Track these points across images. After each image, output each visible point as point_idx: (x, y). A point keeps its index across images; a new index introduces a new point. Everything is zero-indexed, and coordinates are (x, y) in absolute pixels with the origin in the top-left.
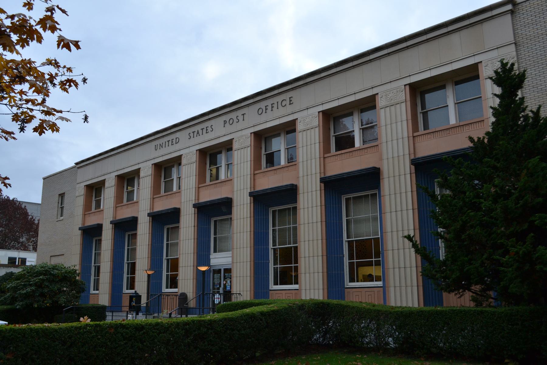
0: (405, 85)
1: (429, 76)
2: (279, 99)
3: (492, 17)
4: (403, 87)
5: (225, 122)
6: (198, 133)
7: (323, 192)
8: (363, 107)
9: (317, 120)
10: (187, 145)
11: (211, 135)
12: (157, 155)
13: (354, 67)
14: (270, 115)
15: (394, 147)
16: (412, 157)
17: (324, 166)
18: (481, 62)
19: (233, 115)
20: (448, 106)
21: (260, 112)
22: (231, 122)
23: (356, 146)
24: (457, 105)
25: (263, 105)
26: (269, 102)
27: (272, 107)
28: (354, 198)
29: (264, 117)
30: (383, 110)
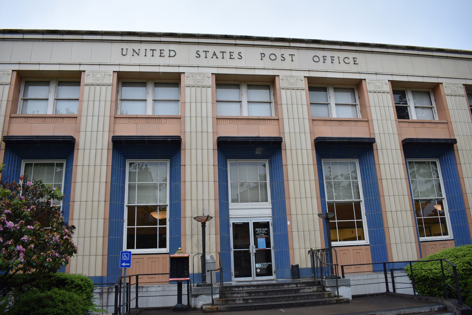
0: (13, 71)
1: (138, 71)
2: (342, 55)
3: (23, 40)
4: (11, 71)
5: (263, 55)
6: (215, 54)
7: (111, 152)
8: (125, 81)
9: (10, 78)
10: (157, 63)
11: (236, 63)
12: (132, 62)
13: (418, 55)
14: (328, 65)
15: (397, 120)
16: (5, 134)
17: (112, 128)
18: (85, 71)
19: (278, 52)
20: (48, 99)
21: (315, 60)
22: (273, 58)
23: (18, 113)
24: (56, 101)
25: (320, 54)
26: (328, 54)
27: (324, 59)
28: (36, 165)
29: (320, 66)
30: (87, 88)
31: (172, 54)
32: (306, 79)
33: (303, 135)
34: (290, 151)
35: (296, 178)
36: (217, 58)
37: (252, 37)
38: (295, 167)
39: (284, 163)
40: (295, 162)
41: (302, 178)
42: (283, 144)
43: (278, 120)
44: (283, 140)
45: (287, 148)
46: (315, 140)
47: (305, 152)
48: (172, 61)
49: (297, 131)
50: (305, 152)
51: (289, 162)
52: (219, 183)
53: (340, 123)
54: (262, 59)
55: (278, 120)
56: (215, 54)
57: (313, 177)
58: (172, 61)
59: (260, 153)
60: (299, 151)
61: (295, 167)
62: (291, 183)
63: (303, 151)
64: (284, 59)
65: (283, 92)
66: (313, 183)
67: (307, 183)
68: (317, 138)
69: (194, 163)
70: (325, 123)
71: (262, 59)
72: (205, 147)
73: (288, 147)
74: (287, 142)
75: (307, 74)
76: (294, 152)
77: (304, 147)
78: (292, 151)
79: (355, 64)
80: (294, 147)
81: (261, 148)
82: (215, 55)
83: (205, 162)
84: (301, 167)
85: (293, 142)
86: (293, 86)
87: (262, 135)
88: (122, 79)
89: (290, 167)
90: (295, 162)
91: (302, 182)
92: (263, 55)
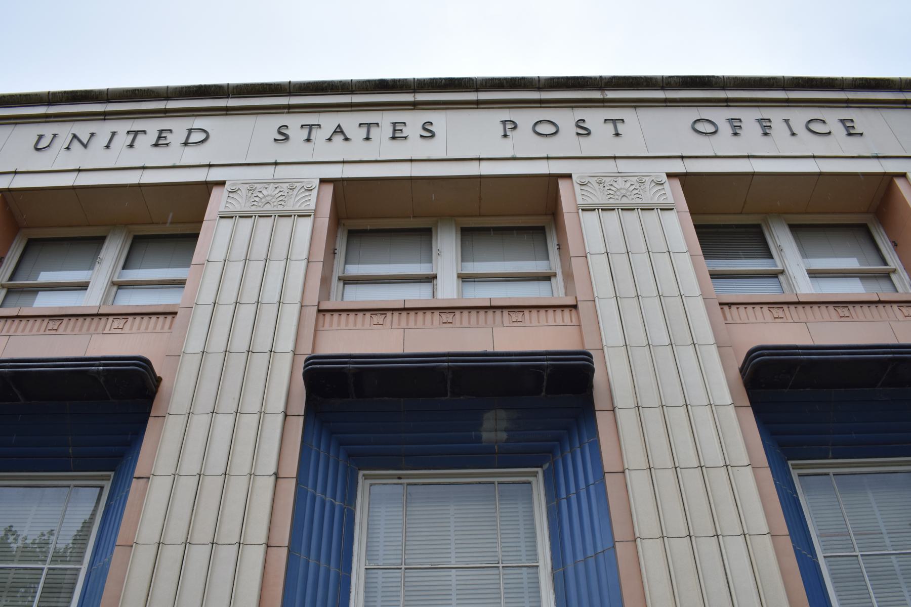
31: (196, 137)
32: (677, 183)
33: (686, 354)
34: (633, 413)
35: (676, 525)
36: (347, 139)
37: (470, 79)
38: (666, 479)
39: (609, 461)
40: (661, 457)
41: (702, 525)
42: (598, 378)
43: (575, 307)
44: (597, 366)
45: (618, 403)
46: (742, 370)
47: (702, 416)
48: (191, 156)
49: (660, 336)
50: (702, 416)
51: (634, 457)
52: (289, 551)
53: (843, 311)
54: (505, 136)
55: (575, 307)
56: (339, 130)
57: (758, 521)
58: (191, 156)
59: (504, 436)
60: (678, 416)
61: (666, 479)
62: (651, 554)
63: (684, 474)
64: (583, 131)
65: (590, 220)
66: (765, 547)
67: (735, 548)
68: (750, 352)
69: (191, 465)
70: (777, 312)
71: (505, 136)
72: (252, 403)
73: (623, 397)
74: (614, 375)
75: (678, 167)
76: (653, 418)
77: (697, 396)
78: (645, 413)
79: (850, 134)
80: (649, 398)
81: (502, 414)
82: (342, 132)
83: (242, 464)
84: (692, 479)
85: (645, 380)
86: (625, 200)
87: (500, 348)
88: (28, 227)
89: (638, 482)
90: (661, 457)
91: (707, 547)
92: (509, 126)
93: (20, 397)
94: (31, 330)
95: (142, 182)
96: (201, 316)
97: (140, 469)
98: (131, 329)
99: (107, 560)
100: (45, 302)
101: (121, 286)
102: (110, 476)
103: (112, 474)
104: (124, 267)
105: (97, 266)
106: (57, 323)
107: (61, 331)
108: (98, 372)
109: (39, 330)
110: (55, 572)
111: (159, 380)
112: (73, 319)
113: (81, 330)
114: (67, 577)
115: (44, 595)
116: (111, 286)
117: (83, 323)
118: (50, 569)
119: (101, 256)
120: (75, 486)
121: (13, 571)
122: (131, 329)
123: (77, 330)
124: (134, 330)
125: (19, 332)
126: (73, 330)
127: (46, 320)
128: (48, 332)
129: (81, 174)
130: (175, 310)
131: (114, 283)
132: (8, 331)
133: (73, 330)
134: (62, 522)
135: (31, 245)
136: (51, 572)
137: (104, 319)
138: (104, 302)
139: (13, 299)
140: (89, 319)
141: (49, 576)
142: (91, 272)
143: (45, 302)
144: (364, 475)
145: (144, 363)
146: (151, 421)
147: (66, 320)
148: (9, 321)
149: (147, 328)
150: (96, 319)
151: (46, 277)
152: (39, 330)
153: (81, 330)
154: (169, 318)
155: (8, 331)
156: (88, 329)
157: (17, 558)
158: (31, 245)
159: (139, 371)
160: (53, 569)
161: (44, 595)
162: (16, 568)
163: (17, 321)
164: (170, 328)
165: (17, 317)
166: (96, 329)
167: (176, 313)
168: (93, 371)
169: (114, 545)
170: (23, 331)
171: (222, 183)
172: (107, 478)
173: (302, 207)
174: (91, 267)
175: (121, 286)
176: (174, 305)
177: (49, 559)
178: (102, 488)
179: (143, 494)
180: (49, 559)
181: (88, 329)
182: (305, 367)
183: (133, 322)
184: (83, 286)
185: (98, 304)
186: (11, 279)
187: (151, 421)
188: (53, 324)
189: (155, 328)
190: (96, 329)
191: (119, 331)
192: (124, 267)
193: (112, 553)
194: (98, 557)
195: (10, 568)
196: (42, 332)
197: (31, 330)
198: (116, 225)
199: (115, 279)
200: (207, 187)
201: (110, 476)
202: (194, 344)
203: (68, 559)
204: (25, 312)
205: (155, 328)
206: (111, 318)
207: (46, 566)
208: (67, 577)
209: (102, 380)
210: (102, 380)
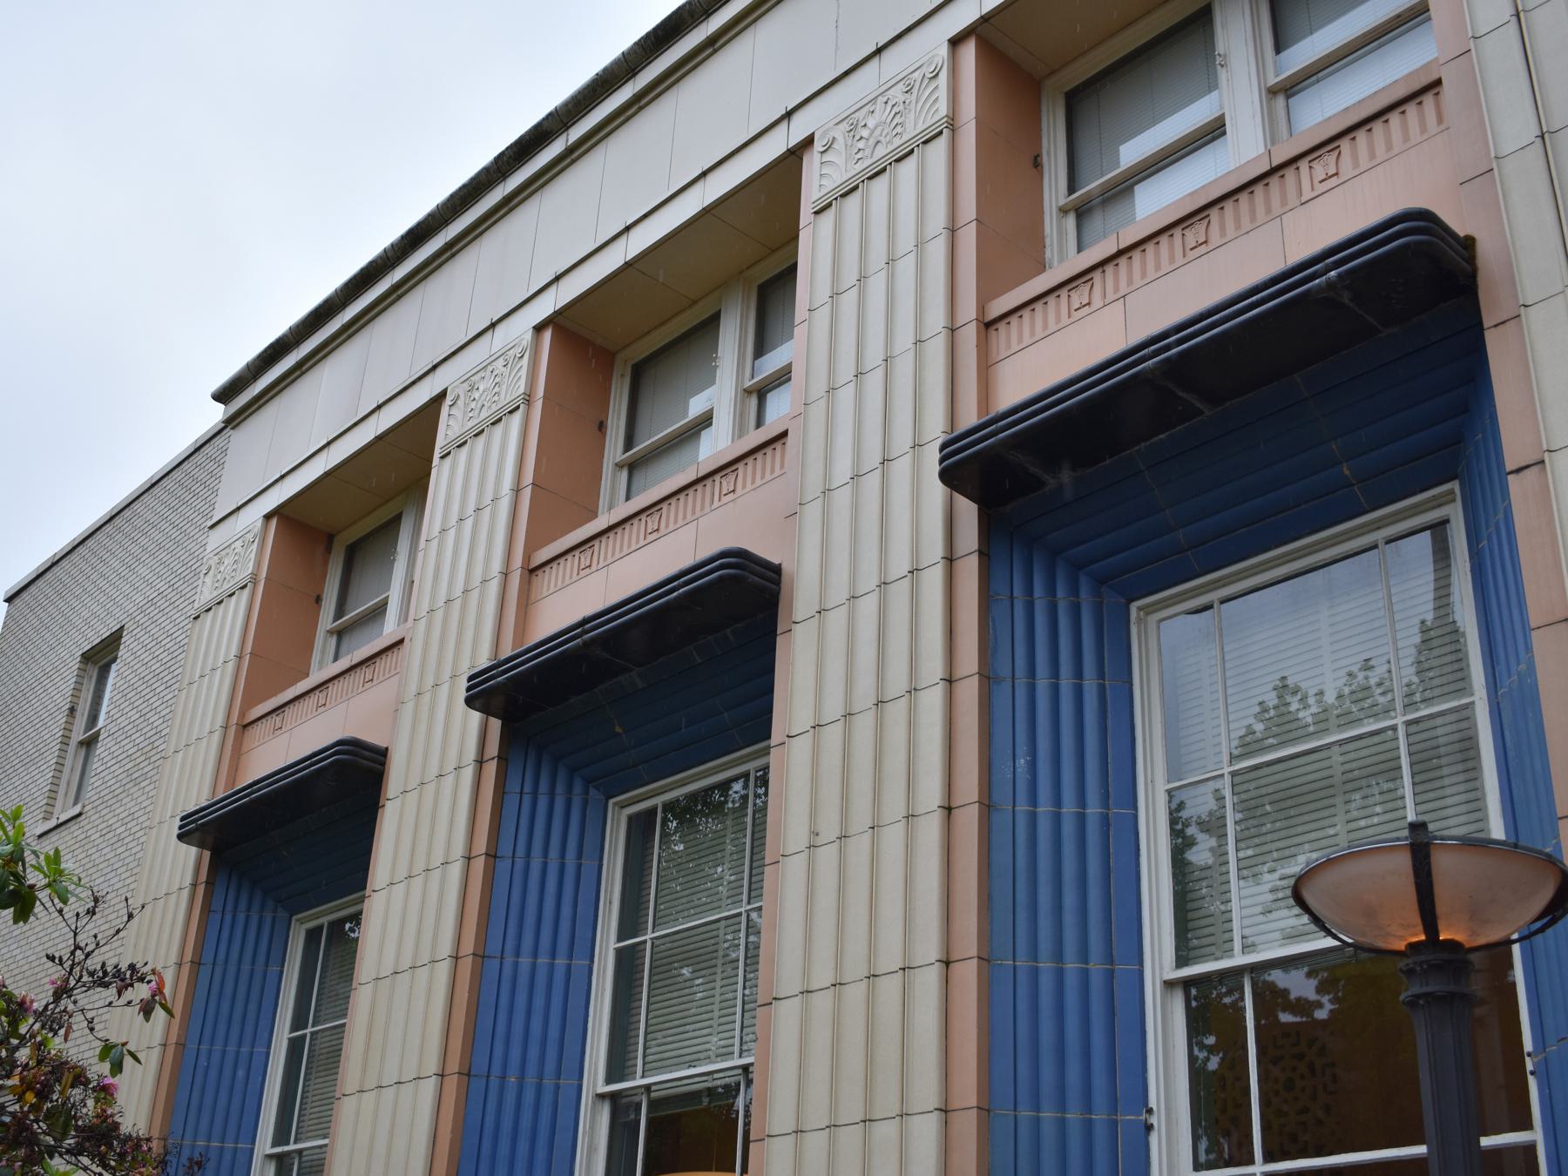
88: (1053, 73)
93: (1198, 405)
94: (1144, 274)
95: (986, 10)
96: (1500, 56)
97: (1514, 450)
98: (1356, 164)
99: (1523, 667)
100: (1156, 201)
101: (1290, 88)
102: (1452, 492)
103: (1455, 485)
104: (1279, 48)
105: (1223, 75)
106: (1201, 227)
107: (1215, 239)
108: (1330, 285)
109: (1172, 259)
110: (1422, 726)
111: (1469, 243)
112: (1229, 205)
113: (1253, 218)
114: (1440, 731)
115: (1418, 779)
116: (1269, 101)
117: (1252, 202)
118: (1408, 723)
119: (1220, 47)
120: (1389, 541)
121: (723, 923)
122: (1356, 164)
123: (1246, 224)
124: (1364, 163)
125: (1138, 282)
126: (1238, 226)
127: (1177, 232)
128: (1191, 255)
129: (886, 55)
130: (1434, 77)
131: (1273, 92)
132: (1116, 289)
133: (1238, 226)
134: (1393, 623)
135: (1075, 101)
136: (1414, 728)
137: (1289, 173)
138: (1272, 137)
139: (1096, 223)
140: (1259, 189)
141: (1412, 739)
142: (1215, 94)
143: (1156, 201)
144: (1140, 609)
145: (1421, 221)
146: (1496, 345)
147: (1214, 213)
148: (1109, 269)
149: (1389, 148)
150: (1274, 181)
151: (1132, 152)
152: (1172, 259)
153: (1253, 218)
154: (1428, 100)
155: (1116, 289)
156: (1268, 210)
157: (1333, 721)
158: (1075, 101)
159: (1416, 243)
160: (1416, 721)
161: (1418, 779)
162: (1341, 743)
163: (1123, 261)
164: (1440, 120)
165: (1120, 253)
166: (1284, 202)
167: (1438, 82)
168: (1319, 288)
169: (1526, 630)
170: (1158, 267)
171: (809, 142)
172: (1448, 498)
173: (920, 127)
174: (1212, 85)
175: (1290, 88)
176: (1426, 66)
177: (1399, 705)
178: (1439, 529)
179: (1544, 496)
180: (1399, 705)
181: (1268, 210)
182: (468, 689)
183: (1222, 218)
184: (1214, 131)
185: (1262, 150)
186: (1072, 189)
187: (1491, 338)
188: (1194, 234)
189: (1406, 138)
190: (1284, 202)
191: (1203, 249)
192: (1279, 48)
193: (1528, 648)
194: (1501, 668)
195: (1328, 746)
196: (1180, 260)
197: (1144, 274)
198: (722, 287)
199: (1272, 80)
200: (795, 155)
201: (1452, 492)
202: (1513, 126)
203: (1311, 729)
204: (1130, 236)
205: (1406, 138)
206: (1303, 165)
207: (1399, 721)
208: (1440, 731)
209: (1346, 298)
210: (1346, 298)
